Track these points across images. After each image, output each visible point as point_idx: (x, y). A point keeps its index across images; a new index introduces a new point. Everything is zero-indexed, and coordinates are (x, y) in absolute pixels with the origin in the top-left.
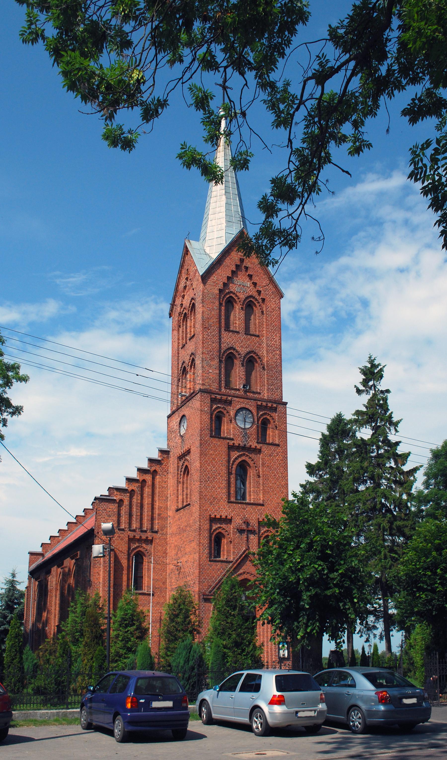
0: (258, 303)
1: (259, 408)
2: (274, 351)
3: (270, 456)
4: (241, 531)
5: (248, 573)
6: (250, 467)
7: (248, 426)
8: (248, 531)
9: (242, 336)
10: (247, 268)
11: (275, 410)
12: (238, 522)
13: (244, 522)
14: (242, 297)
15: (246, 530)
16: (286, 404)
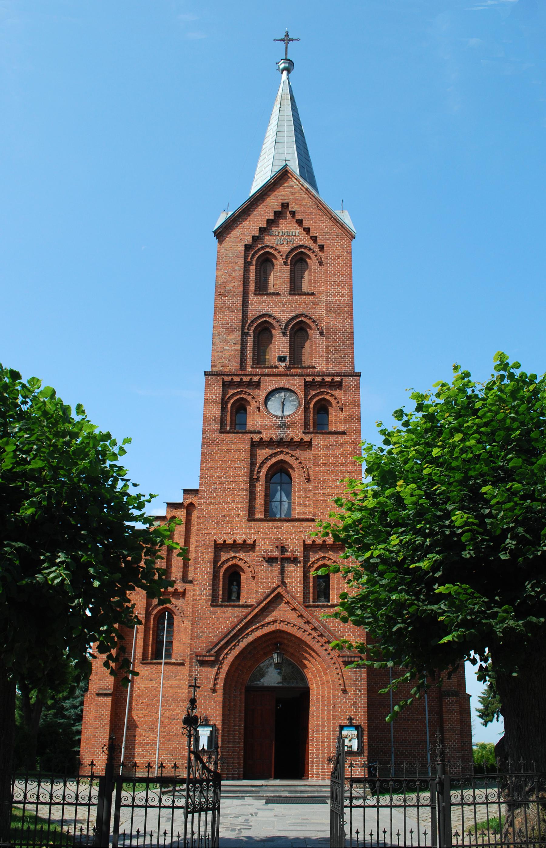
0: (314, 252)
1: (308, 386)
2: (339, 308)
3: (328, 449)
4: (270, 560)
5: (281, 621)
6: (292, 468)
8: (283, 559)
9: (285, 298)
10: (293, 213)
11: (339, 385)
12: (266, 546)
13: (277, 547)
14: (286, 249)
15: (281, 558)
16: (359, 375)
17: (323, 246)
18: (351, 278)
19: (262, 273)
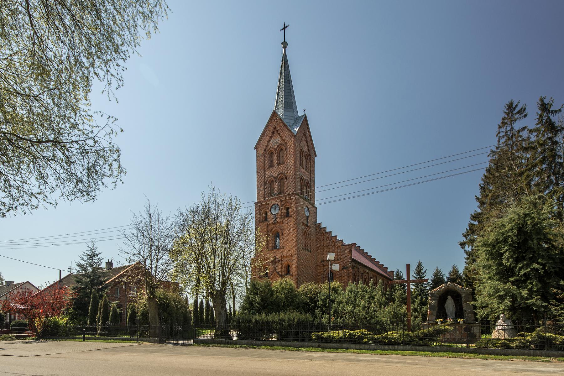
7: (276, 213)
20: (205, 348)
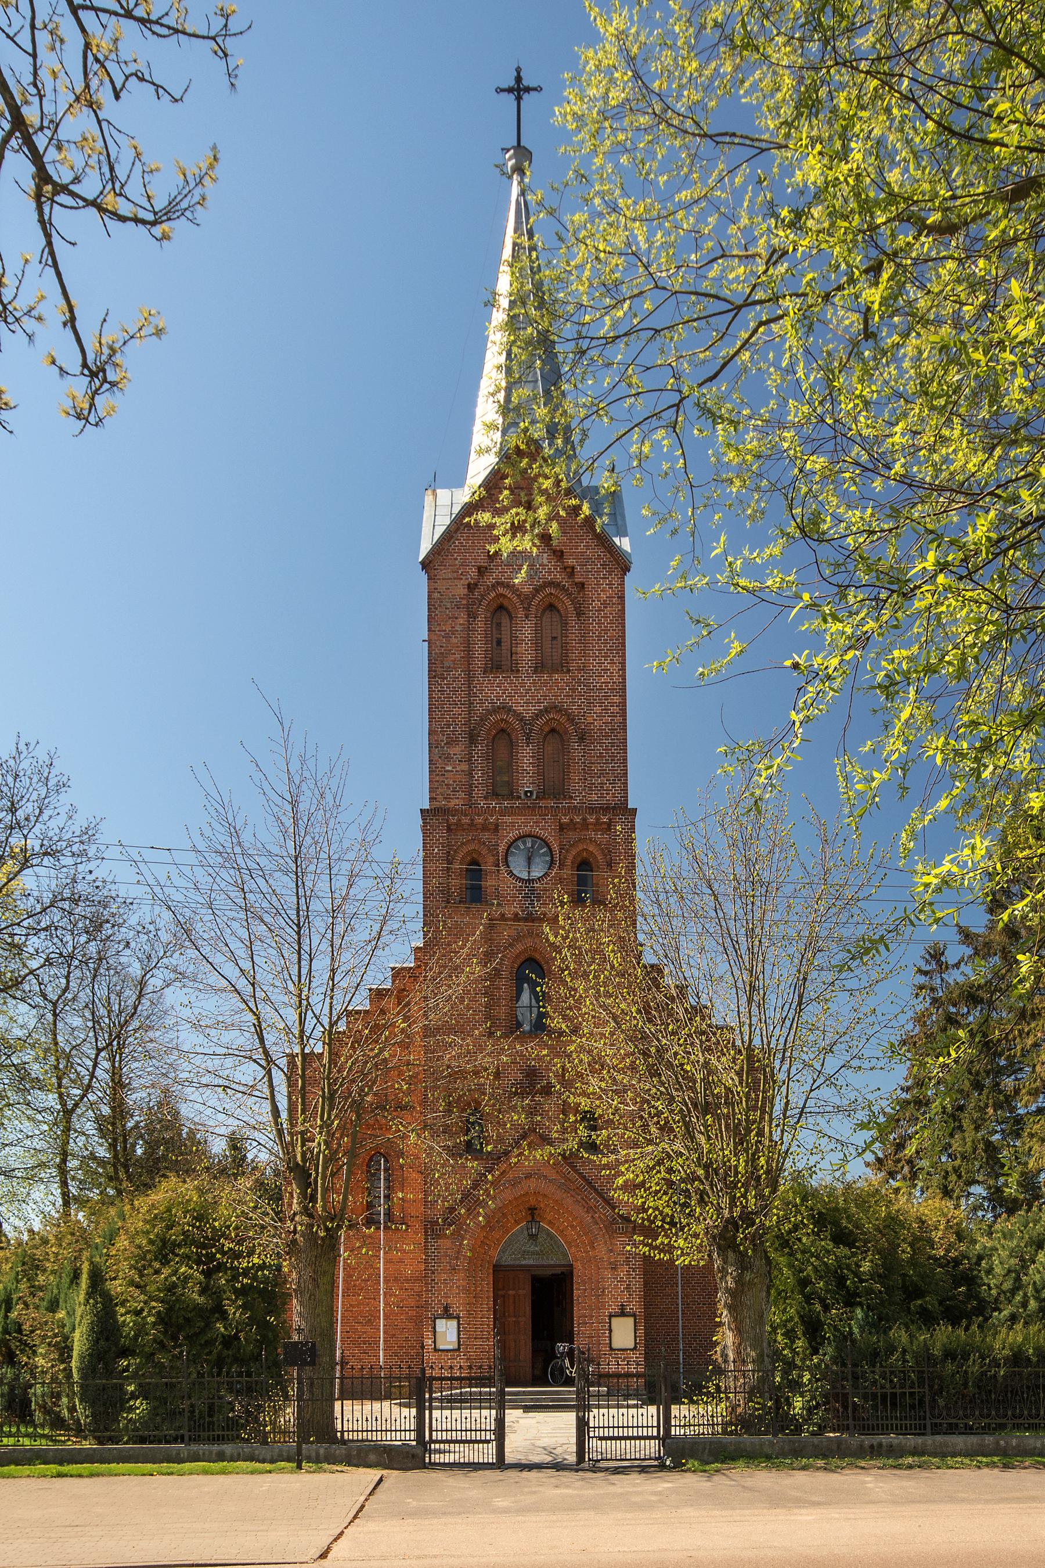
7: (536, 873)
17: (583, 584)
18: (623, 644)
19: (755, 1009)
20: (717, 1478)
